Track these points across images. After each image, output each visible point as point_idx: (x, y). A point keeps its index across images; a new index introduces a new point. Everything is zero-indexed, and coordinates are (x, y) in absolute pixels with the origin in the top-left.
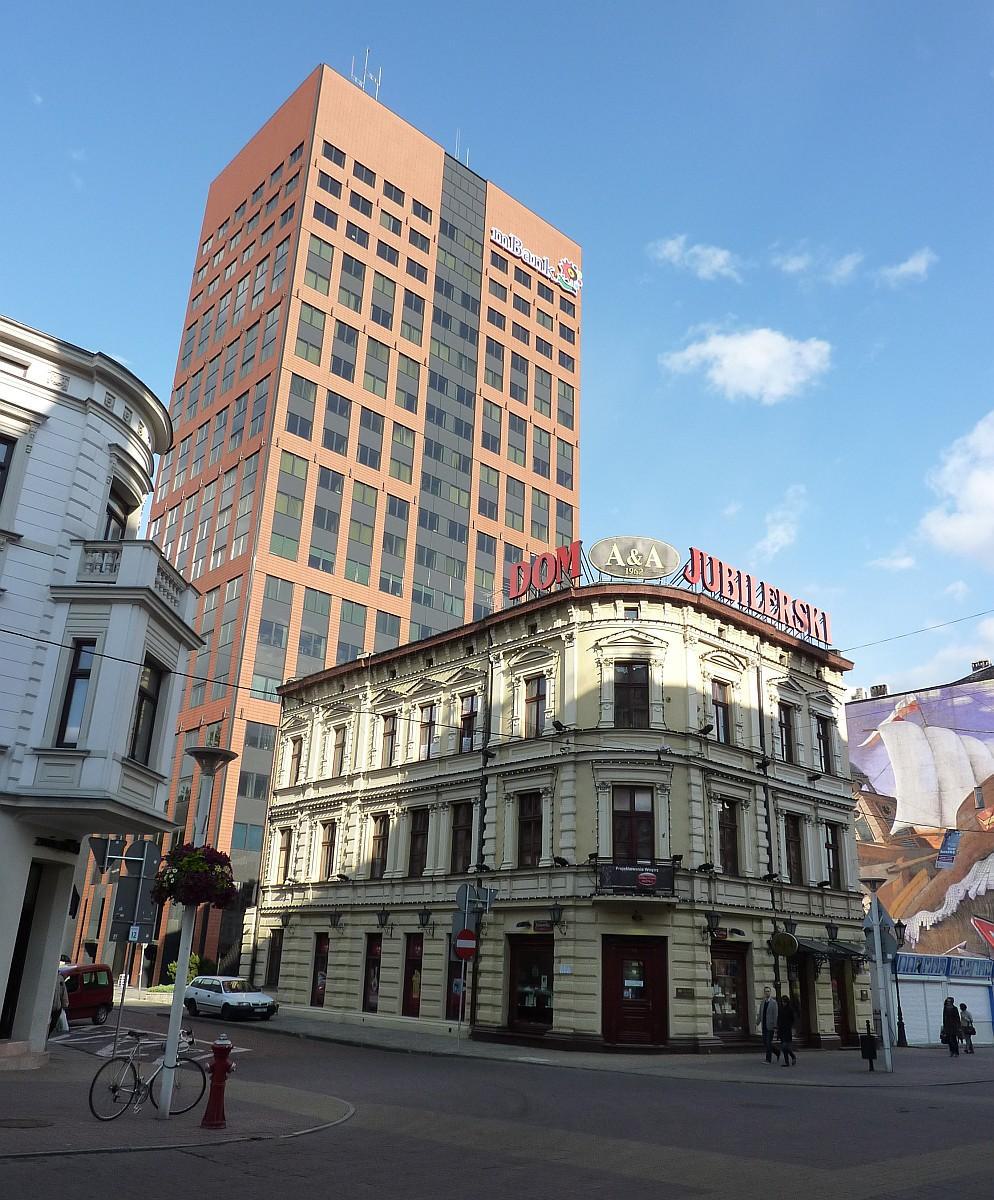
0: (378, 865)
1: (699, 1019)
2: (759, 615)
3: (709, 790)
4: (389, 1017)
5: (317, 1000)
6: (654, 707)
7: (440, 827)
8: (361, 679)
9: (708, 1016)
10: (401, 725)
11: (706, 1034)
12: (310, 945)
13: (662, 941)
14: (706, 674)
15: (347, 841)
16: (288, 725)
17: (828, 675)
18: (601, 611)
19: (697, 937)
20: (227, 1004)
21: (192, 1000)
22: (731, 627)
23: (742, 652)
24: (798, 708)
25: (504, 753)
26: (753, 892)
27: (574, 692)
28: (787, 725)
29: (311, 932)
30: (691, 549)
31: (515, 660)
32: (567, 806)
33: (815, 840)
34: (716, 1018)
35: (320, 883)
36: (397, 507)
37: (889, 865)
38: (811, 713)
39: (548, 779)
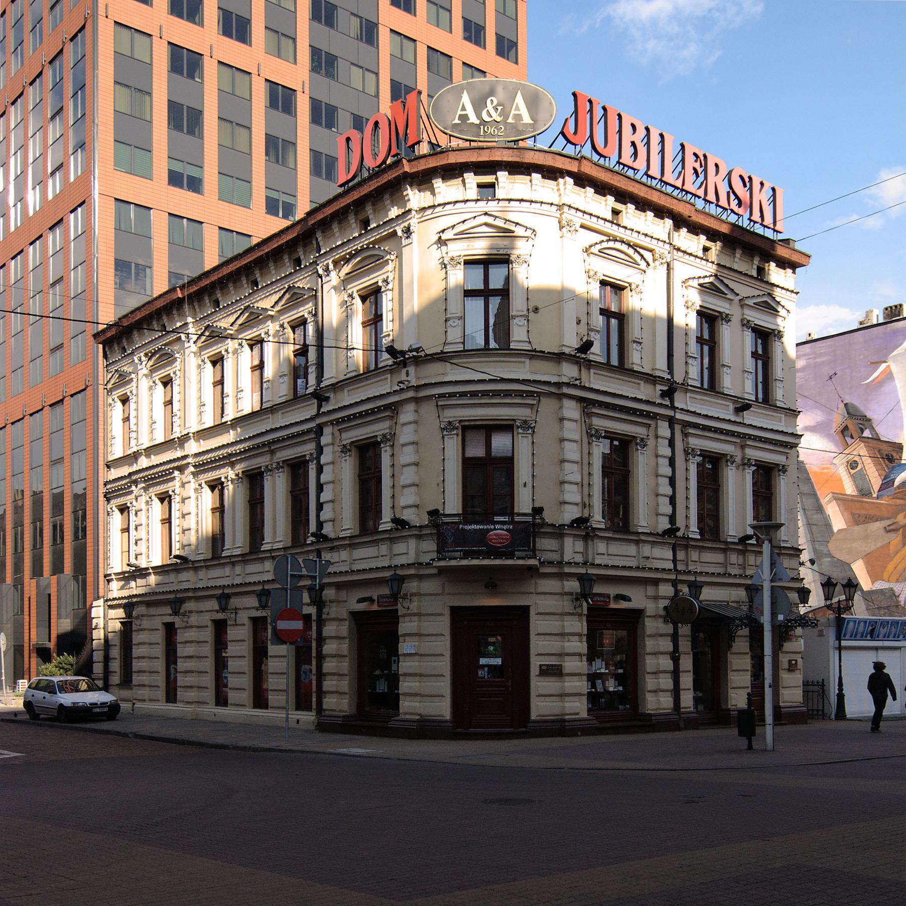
0: (217, 540)
1: (567, 699)
2: (677, 192)
3: (590, 427)
4: (240, 709)
5: (171, 696)
6: (516, 321)
7: (276, 489)
8: (182, 315)
9: (580, 695)
10: (229, 364)
11: (577, 714)
12: (159, 637)
13: (525, 610)
14: (591, 274)
15: (183, 516)
16: (112, 381)
17: (775, 274)
18: (445, 190)
19: (567, 605)
20: (61, 705)
21: (30, 702)
22: (631, 207)
23: (652, 244)
24: (727, 318)
25: (340, 395)
26: (646, 550)
27: (415, 303)
28: (709, 341)
29: (158, 623)
30: (574, 95)
31: (347, 269)
32: (407, 455)
33: (737, 488)
34: (593, 697)
35: (163, 566)
36: (281, 98)
37: (888, 522)
38: (745, 324)
39: (387, 424)
